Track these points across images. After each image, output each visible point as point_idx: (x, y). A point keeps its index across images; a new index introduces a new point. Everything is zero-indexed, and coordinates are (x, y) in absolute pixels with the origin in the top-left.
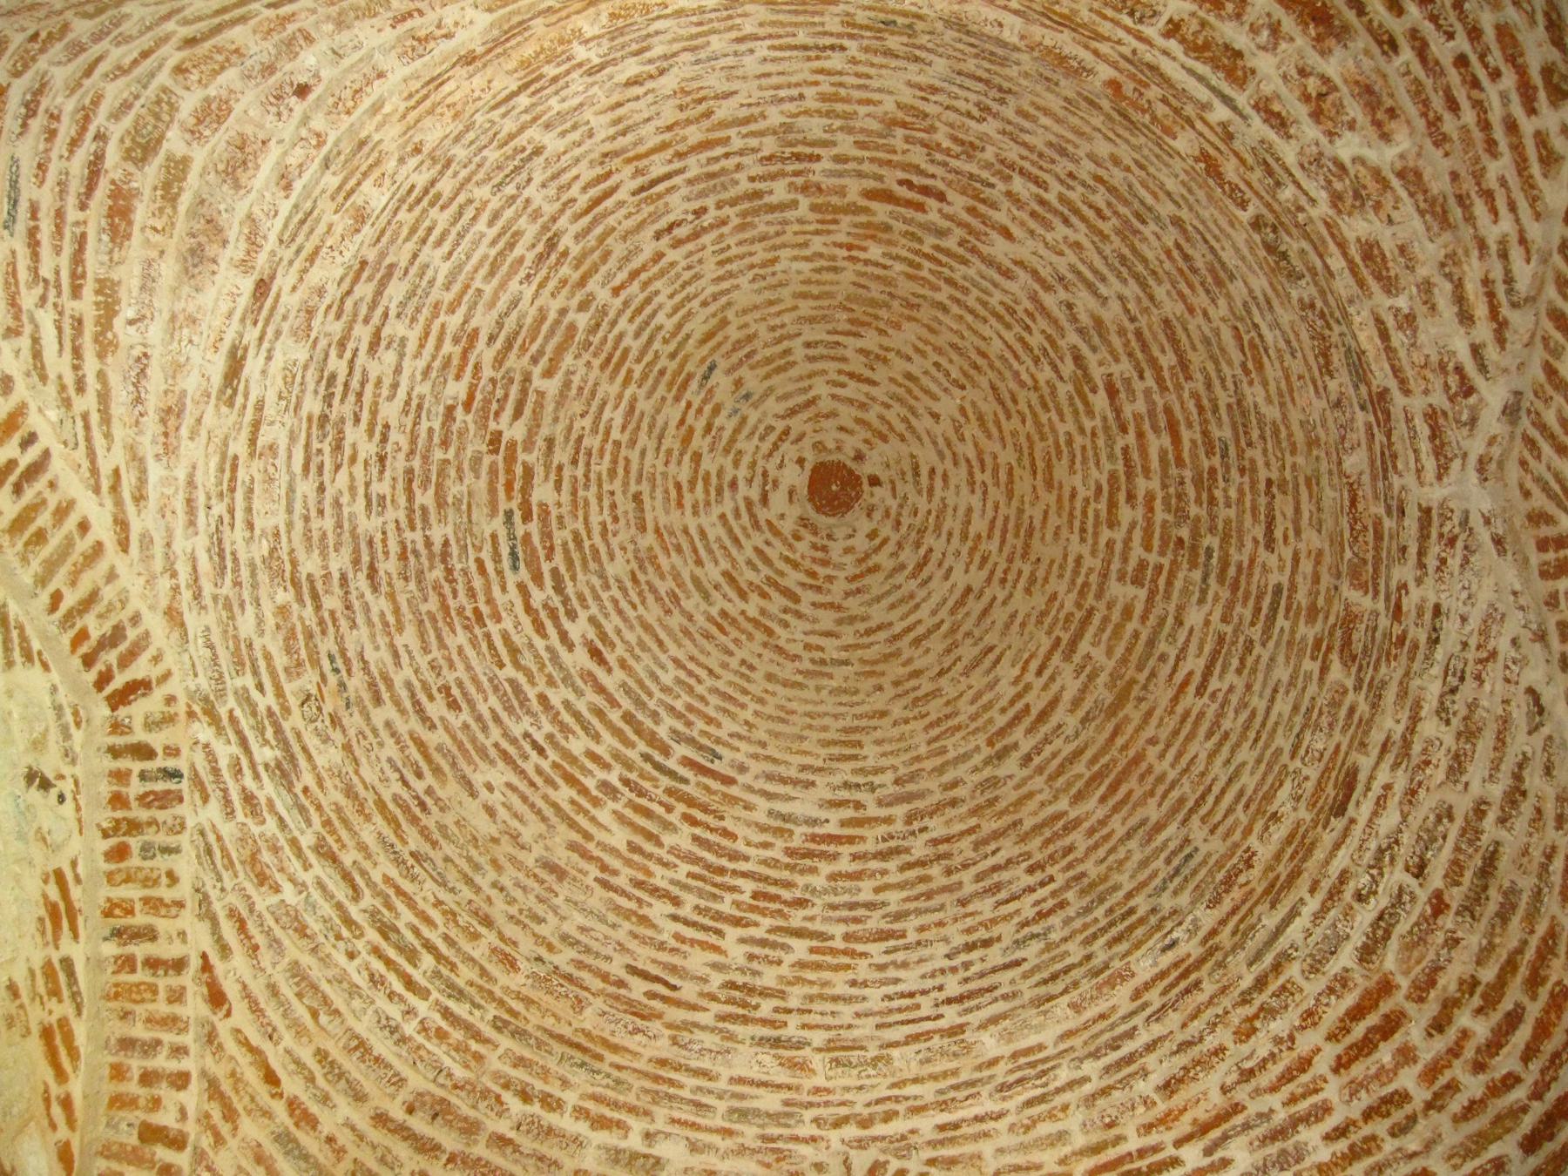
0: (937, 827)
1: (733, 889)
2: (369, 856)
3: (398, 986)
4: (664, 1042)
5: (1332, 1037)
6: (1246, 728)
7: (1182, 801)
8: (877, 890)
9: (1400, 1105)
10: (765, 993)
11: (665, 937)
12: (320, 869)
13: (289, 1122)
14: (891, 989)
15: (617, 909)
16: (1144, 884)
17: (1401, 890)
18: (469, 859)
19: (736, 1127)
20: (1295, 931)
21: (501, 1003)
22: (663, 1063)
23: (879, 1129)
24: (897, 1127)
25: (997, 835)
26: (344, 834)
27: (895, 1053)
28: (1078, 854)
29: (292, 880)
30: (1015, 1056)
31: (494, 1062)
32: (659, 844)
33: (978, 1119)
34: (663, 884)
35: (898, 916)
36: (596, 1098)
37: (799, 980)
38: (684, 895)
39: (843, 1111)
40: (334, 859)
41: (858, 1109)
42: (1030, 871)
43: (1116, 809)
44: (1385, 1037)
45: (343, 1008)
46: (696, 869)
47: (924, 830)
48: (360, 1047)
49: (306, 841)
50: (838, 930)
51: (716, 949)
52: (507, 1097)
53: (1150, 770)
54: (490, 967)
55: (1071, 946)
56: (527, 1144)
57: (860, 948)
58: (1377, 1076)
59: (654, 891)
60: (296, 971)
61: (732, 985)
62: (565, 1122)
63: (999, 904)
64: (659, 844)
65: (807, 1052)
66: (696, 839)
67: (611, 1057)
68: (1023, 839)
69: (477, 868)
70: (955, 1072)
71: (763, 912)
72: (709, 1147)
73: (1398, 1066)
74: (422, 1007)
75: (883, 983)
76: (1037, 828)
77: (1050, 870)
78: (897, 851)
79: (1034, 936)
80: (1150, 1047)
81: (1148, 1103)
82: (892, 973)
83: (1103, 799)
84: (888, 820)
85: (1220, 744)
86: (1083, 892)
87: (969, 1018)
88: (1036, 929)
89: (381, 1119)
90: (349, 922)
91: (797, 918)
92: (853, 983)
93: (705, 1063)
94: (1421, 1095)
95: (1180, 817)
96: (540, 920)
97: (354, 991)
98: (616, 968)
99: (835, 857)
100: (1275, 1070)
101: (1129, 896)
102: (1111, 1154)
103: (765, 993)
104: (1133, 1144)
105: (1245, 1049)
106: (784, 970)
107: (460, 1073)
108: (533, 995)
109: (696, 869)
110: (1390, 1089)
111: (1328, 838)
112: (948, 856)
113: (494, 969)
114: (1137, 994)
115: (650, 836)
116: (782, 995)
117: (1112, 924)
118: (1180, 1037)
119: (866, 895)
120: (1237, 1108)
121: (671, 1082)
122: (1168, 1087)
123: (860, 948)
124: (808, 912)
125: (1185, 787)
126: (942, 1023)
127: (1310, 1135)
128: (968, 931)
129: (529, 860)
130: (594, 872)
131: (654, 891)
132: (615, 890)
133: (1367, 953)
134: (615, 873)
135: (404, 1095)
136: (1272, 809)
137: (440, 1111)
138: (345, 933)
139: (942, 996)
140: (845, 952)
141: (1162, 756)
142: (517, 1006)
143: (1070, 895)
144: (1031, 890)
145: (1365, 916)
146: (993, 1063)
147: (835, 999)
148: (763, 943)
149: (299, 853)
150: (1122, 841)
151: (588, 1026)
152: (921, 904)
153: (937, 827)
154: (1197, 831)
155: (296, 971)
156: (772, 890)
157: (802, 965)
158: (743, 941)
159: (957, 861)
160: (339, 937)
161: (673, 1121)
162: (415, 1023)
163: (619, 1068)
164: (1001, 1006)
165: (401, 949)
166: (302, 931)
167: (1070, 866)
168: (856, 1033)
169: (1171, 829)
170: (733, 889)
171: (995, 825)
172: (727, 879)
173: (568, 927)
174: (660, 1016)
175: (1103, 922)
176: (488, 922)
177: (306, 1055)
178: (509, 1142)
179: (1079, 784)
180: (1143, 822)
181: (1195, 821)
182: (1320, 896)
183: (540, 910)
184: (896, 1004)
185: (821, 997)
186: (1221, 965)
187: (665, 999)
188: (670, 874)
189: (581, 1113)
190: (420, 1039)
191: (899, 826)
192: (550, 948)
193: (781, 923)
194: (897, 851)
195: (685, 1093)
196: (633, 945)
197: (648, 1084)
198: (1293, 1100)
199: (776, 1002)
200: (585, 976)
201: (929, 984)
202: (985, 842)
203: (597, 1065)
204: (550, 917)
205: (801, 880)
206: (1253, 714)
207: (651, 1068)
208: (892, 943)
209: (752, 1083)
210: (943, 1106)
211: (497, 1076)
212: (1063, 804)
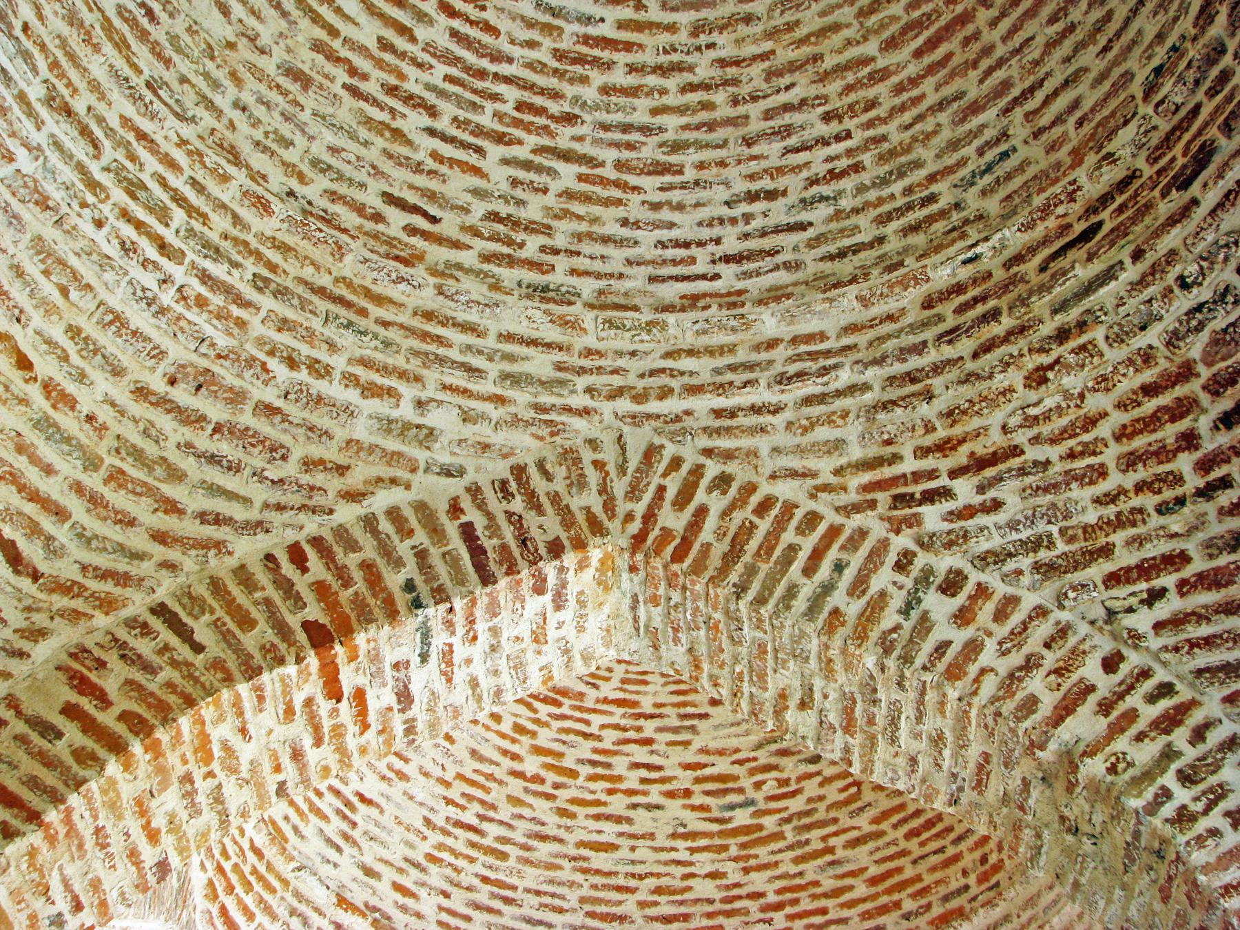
0: (726, 45)
1: (495, 97)
2: (102, 97)
3: (152, 253)
4: (430, 292)
5: (1121, 406)
6: (1098, 28)
7: (1006, 85)
8: (655, 112)
9: (1171, 486)
10: (531, 228)
11: (420, 156)
12: (55, 125)
13: (46, 405)
14: (665, 235)
15: (368, 122)
16: (949, 170)
17: (1227, 289)
18: (206, 75)
19: (509, 393)
20: (1106, 293)
21: (258, 256)
22: (429, 316)
23: (654, 406)
24: (672, 405)
25: (794, 67)
26: (73, 74)
27: (671, 318)
28: (880, 111)
29: (26, 145)
30: (795, 340)
31: (257, 327)
32: (413, 40)
33: (755, 410)
34: (417, 89)
35: (677, 147)
36: (365, 363)
37: (566, 214)
38: (441, 104)
39: (617, 381)
40: (68, 112)
41: (631, 380)
42: (827, 118)
43: (931, 70)
44: (1173, 420)
45: (94, 282)
46: (454, 72)
47: (710, 46)
48: (117, 321)
49: (35, 92)
50: (610, 155)
51: (477, 171)
52: (273, 364)
53: (976, 36)
54: (244, 213)
55: (863, 221)
56: (295, 411)
57: (633, 180)
58: (1156, 454)
59: (409, 99)
60: (39, 246)
61: (494, 217)
62: (334, 390)
63: (788, 151)
64: (413, 40)
65: (577, 309)
66: (454, 34)
67: (375, 311)
68: (823, 78)
69: (216, 85)
70: (732, 349)
71: (527, 127)
72: (483, 417)
73: (1179, 449)
74: (178, 273)
75: (657, 225)
76: (840, 69)
77: (849, 124)
78: (678, 68)
79: (823, 199)
80: (937, 369)
81: (929, 428)
82: (666, 215)
83: (918, 54)
84: (672, 28)
85: (1064, 34)
86: (881, 158)
87: (751, 284)
88: (825, 190)
89: (141, 392)
90: (93, 185)
91: (564, 137)
92: (625, 222)
93: (472, 316)
94: (1194, 481)
95: (1003, 103)
96: (288, 144)
97: (105, 262)
98: (372, 200)
99: (609, 66)
100: (1060, 423)
101: (932, 178)
102: (887, 472)
103: (531, 228)
104: (909, 465)
105: (1033, 396)
106: (550, 200)
107: (222, 341)
108: (291, 240)
109: (454, 72)
110: (1167, 467)
111: (1164, 209)
112: (735, 82)
113: (246, 214)
114: (928, 304)
115: (403, 30)
116: (547, 230)
117: (909, 207)
118: (970, 366)
119: (641, 117)
120: (1016, 451)
121: (439, 340)
122: (950, 415)
123: (633, 180)
124: (578, 130)
125: (1012, 70)
126: (717, 285)
127: (1081, 494)
128: (752, 177)
129: (269, 65)
130: (342, 76)
131: (409, 99)
132: (366, 98)
133: (1173, 339)
134: (365, 77)
135: (165, 367)
136: (1110, 148)
137: (204, 382)
138: (91, 199)
139: (719, 251)
140: (617, 184)
141: (994, 23)
142: (274, 256)
143: (867, 158)
144: (825, 142)
145: (1184, 302)
146: (772, 344)
147: (606, 240)
148: (527, 165)
149: (30, 112)
150: (932, 110)
151: (348, 273)
152: (701, 135)
153: (726, 45)
154: (1019, 130)
155: (39, 246)
156: (539, 101)
157: (569, 194)
158: (506, 162)
159: (745, 90)
160: (84, 205)
161: (445, 387)
162: (172, 291)
163: (386, 324)
164: (782, 277)
165: (150, 210)
166: (44, 203)
167: (870, 124)
168: (627, 284)
169: (990, 115)
170: (495, 97)
171: (793, 54)
172: (487, 84)
173: (318, 149)
174: (421, 257)
175: (900, 202)
176: (235, 156)
177: (57, 333)
178: (277, 411)
179: (894, 28)
180: (959, 96)
181: (1018, 113)
182: (1143, 266)
183: (286, 130)
184: (670, 253)
185: (589, 235)
186: (1023, 301)
187: (425, 235)
188: (425, 77)
189: (350, 380)
190: (179, 308)
191: (682, 37)
192: (301, 177)
193: (546, 141)
194: (678, 68)
195: (454, 354)
196: (387, 166)
197: (416, 344)
198: (1072, 455)
199: (541, 240)
200: (339, 209)
201: (705, 233)
202: (779, 73)
203: (362, 323)
204: (299, 139)
205: (570, 90)
206: (1108, 17)
207: (417, 323)
208: (668, 179)
209: (522, 341)
210: (721, 388)
211: (261, 342)
212: (871, 48)
